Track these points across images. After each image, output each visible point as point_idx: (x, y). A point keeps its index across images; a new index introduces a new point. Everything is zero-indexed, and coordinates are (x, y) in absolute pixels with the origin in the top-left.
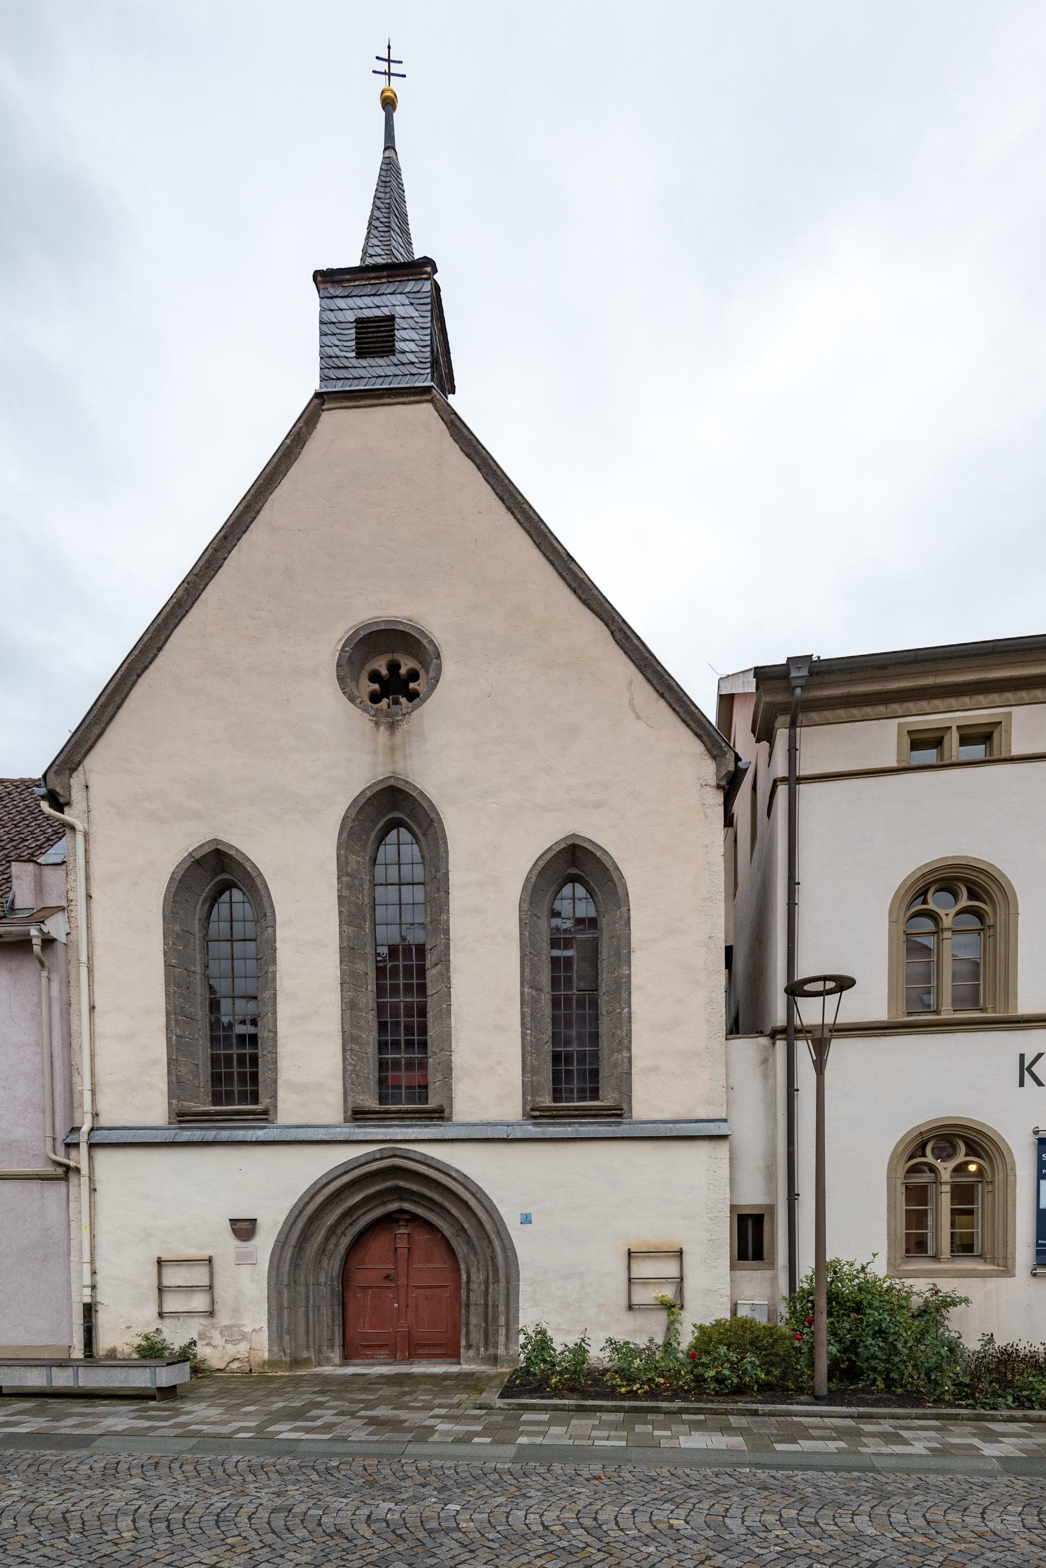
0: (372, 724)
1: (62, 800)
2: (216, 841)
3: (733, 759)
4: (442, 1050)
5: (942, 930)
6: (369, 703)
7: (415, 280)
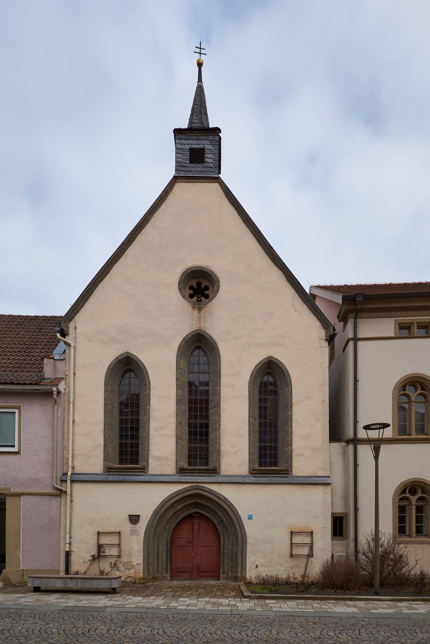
0: (192, 308)
1: (65, 333)
2: (128, 353)
3: (332, 329)
4: (217, 444)
6: (188, 297)
7: (213, 135)
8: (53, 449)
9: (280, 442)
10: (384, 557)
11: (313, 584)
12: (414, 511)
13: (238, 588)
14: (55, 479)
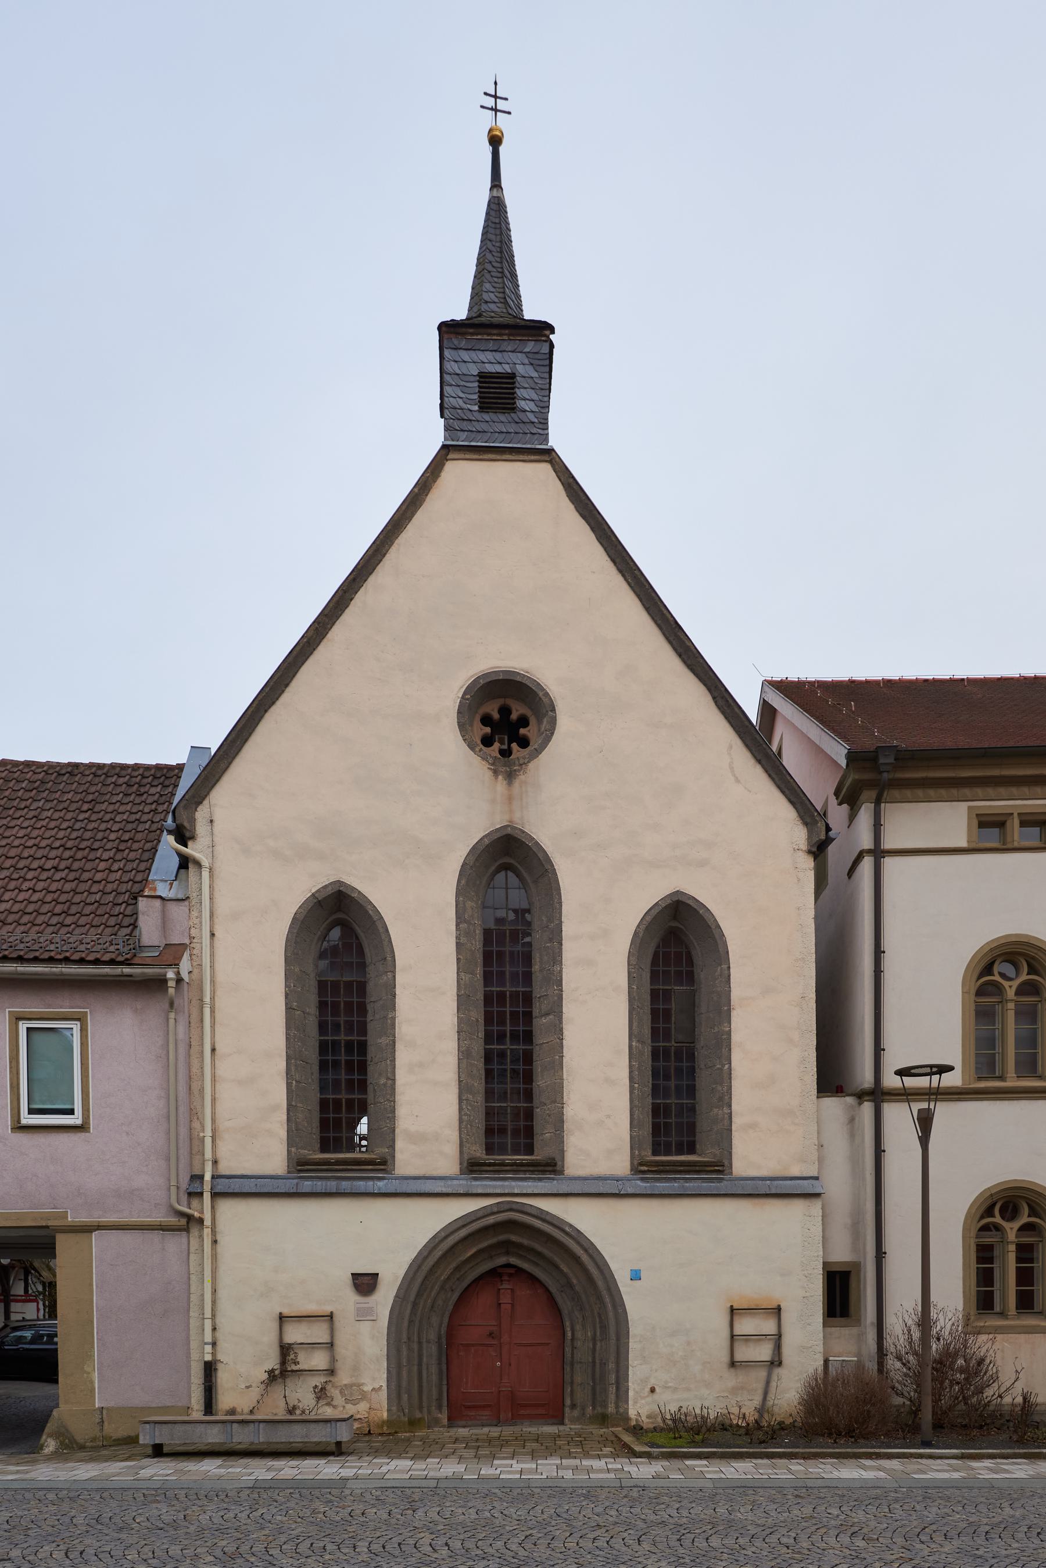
0: (491, 773)
1: (187, 834)
2: (339, 883)
3: (824, 828)
4: (555, 1102)
5: (1007, 1001)
6: (479, 742)
8: (168, 1118)
9: (702, 1095)
10: (943, 1363)
11: (783, 1429)
12: (1012, 1257)
13: (613, 1439)
14: (173, 1190)
